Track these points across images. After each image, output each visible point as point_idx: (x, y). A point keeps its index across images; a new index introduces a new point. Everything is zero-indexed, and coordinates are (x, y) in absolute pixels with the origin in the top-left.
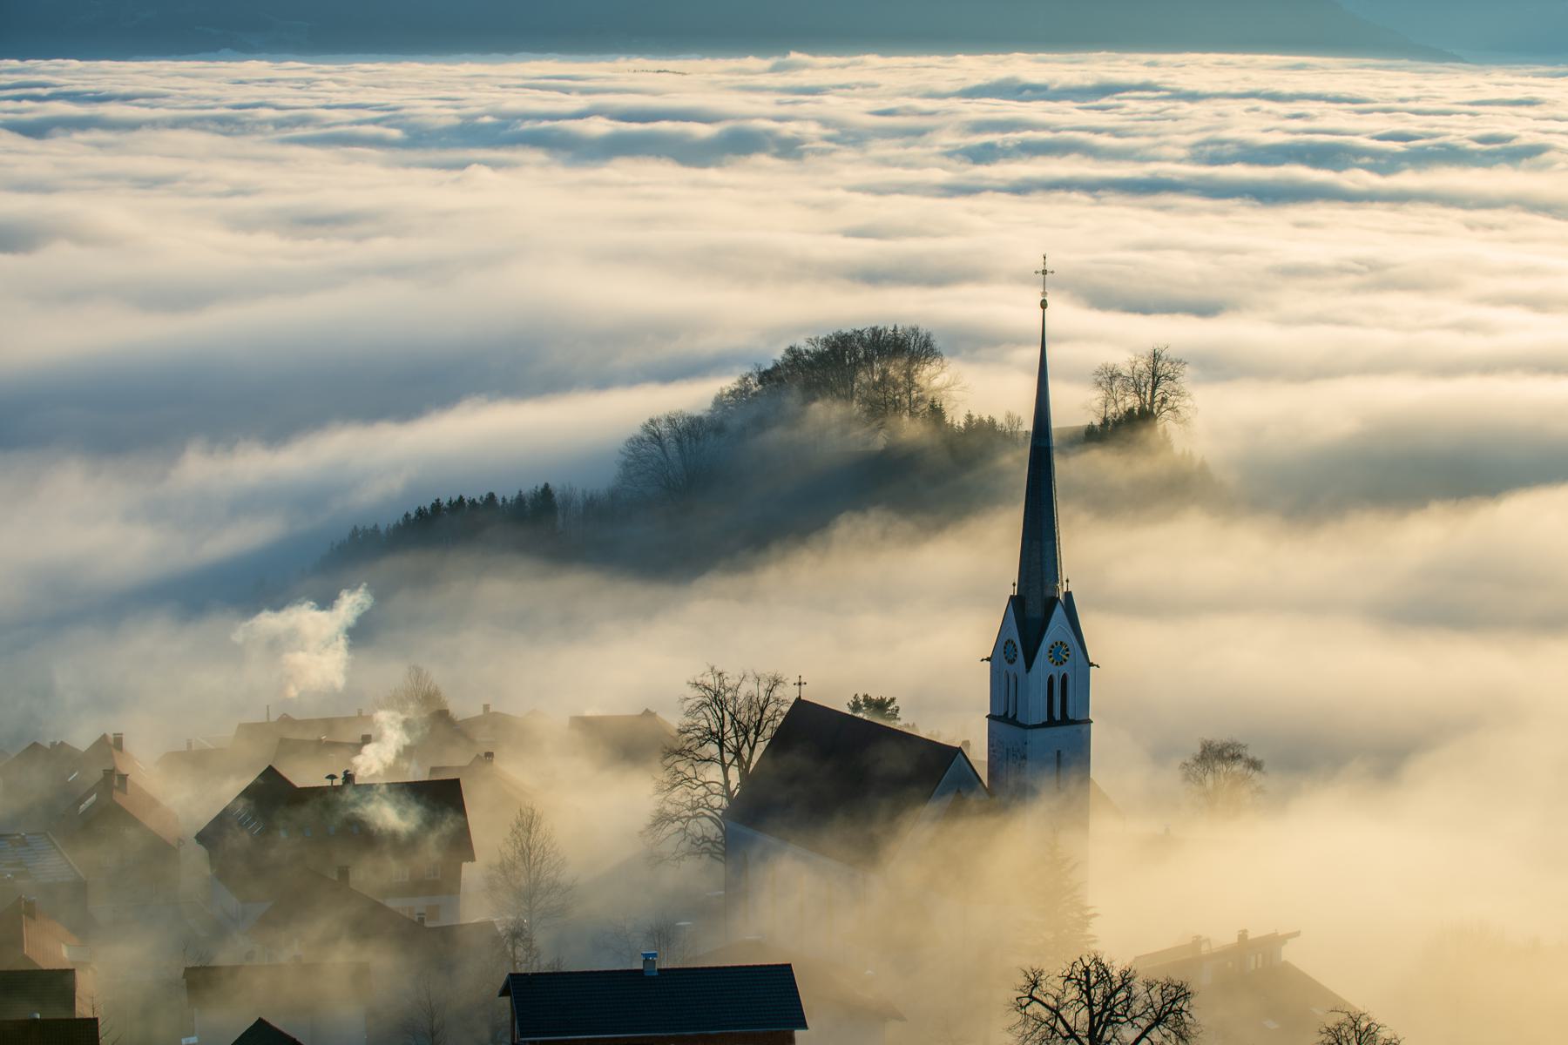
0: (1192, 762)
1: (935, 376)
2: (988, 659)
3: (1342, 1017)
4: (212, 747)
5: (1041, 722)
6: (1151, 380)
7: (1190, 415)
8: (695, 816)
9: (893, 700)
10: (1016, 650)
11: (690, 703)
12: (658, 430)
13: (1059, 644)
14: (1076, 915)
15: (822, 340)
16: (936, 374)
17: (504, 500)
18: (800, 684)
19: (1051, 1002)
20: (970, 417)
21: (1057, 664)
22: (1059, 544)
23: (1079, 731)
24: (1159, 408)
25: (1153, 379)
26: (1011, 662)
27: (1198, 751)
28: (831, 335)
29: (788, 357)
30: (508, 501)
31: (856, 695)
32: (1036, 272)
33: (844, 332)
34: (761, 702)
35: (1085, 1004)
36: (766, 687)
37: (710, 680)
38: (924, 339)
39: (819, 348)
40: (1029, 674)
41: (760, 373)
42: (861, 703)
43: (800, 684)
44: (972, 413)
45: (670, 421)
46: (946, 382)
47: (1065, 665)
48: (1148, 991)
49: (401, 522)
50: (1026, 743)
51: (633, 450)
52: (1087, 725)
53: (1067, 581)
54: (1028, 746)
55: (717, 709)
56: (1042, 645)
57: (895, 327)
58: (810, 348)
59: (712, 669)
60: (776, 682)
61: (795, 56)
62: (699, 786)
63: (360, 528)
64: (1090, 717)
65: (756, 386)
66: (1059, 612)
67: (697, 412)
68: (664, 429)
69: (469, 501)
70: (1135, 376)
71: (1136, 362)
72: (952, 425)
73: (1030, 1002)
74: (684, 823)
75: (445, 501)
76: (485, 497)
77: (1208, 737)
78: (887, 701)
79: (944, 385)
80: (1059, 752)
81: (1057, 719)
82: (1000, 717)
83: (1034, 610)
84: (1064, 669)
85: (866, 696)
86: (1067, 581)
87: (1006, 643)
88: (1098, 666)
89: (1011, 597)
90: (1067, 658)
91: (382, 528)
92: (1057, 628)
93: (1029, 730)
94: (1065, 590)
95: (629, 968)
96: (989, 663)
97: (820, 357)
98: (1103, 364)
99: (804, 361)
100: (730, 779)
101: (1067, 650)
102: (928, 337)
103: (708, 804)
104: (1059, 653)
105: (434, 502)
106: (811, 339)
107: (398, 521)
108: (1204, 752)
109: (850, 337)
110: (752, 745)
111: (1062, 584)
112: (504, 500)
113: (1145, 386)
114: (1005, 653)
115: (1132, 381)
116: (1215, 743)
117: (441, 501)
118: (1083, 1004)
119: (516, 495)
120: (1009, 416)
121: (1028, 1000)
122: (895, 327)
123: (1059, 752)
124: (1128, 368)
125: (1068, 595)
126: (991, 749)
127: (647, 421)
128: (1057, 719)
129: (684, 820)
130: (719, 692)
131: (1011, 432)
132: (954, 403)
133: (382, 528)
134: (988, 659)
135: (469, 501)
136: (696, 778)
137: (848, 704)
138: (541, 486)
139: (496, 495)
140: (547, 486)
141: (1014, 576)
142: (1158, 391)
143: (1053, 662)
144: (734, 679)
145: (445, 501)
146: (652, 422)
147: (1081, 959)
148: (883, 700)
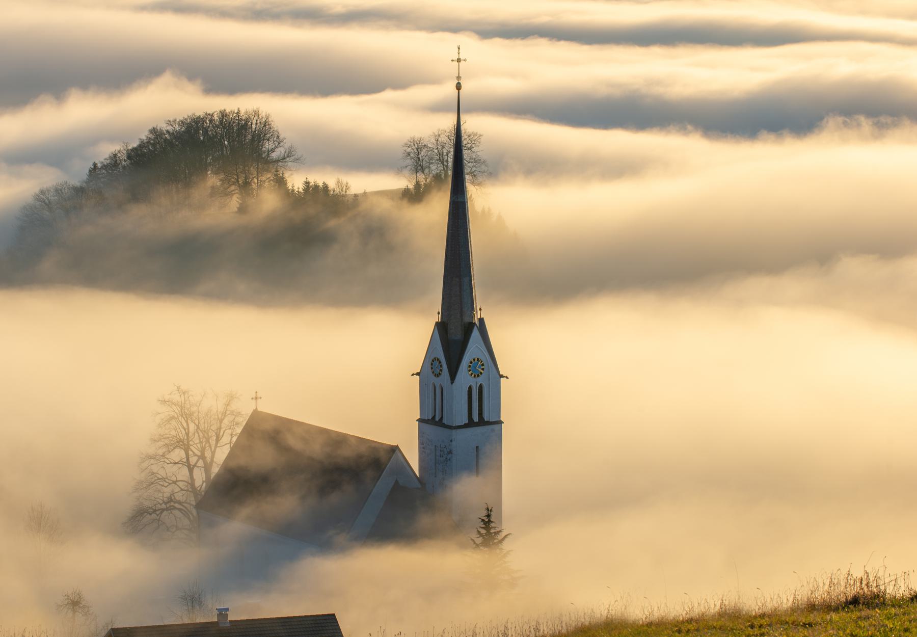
1: (273, 150)
5: (463, 424)
8: (167, 509)
10: (441, 366)
12: (48, 199)
13: (476, 361)
15: (179, 122)
16: (275, 148)
23: (493, 430)
28: (186, 117)
29: (152, 136)
32: (452, 61)
33: (198, 114)
34: (220, 416)
37: (177, 398)
38: (264, 120)
39: (177, 127)
40: (454, 384)
41: (127, 150)
47: (481, 377)
50: (451, 441)
52: (500, 425)
53: (480, 309)
54: (454, 443)
58: (170, 128)
59: (179, 389)
62: (171, 483)
65: (125, 161)
66: (476, 333)
70: (439, 148)
71: (439, 135)
72: (293, 190)
74: (157, 515)
81: (475, 421)
84: (480, 380)
86: (480, 309)
87: (433, 361)
88: (507, 378)
89: (437, 323)
90: (482, 371)
93: (454, 431)
94: (479, 317)
95: (210, 621)
96: (418, 377)
97: (176, 135)
99: (166, 139)
100: (195, 477)
101: (483, 365)
102: (267, 118)
104: (476, 368)
106: (169, 121)
111: (477, 313)
113: (447, 155)
114: (432, 368)
123: (477, 447)
124: (433, 140)
125: (481, 320)
126: (422, 446)
128: (475, 421)
129: (158, 512)
134: (418, 374)
143: (471, 375)
146: (42, 192)
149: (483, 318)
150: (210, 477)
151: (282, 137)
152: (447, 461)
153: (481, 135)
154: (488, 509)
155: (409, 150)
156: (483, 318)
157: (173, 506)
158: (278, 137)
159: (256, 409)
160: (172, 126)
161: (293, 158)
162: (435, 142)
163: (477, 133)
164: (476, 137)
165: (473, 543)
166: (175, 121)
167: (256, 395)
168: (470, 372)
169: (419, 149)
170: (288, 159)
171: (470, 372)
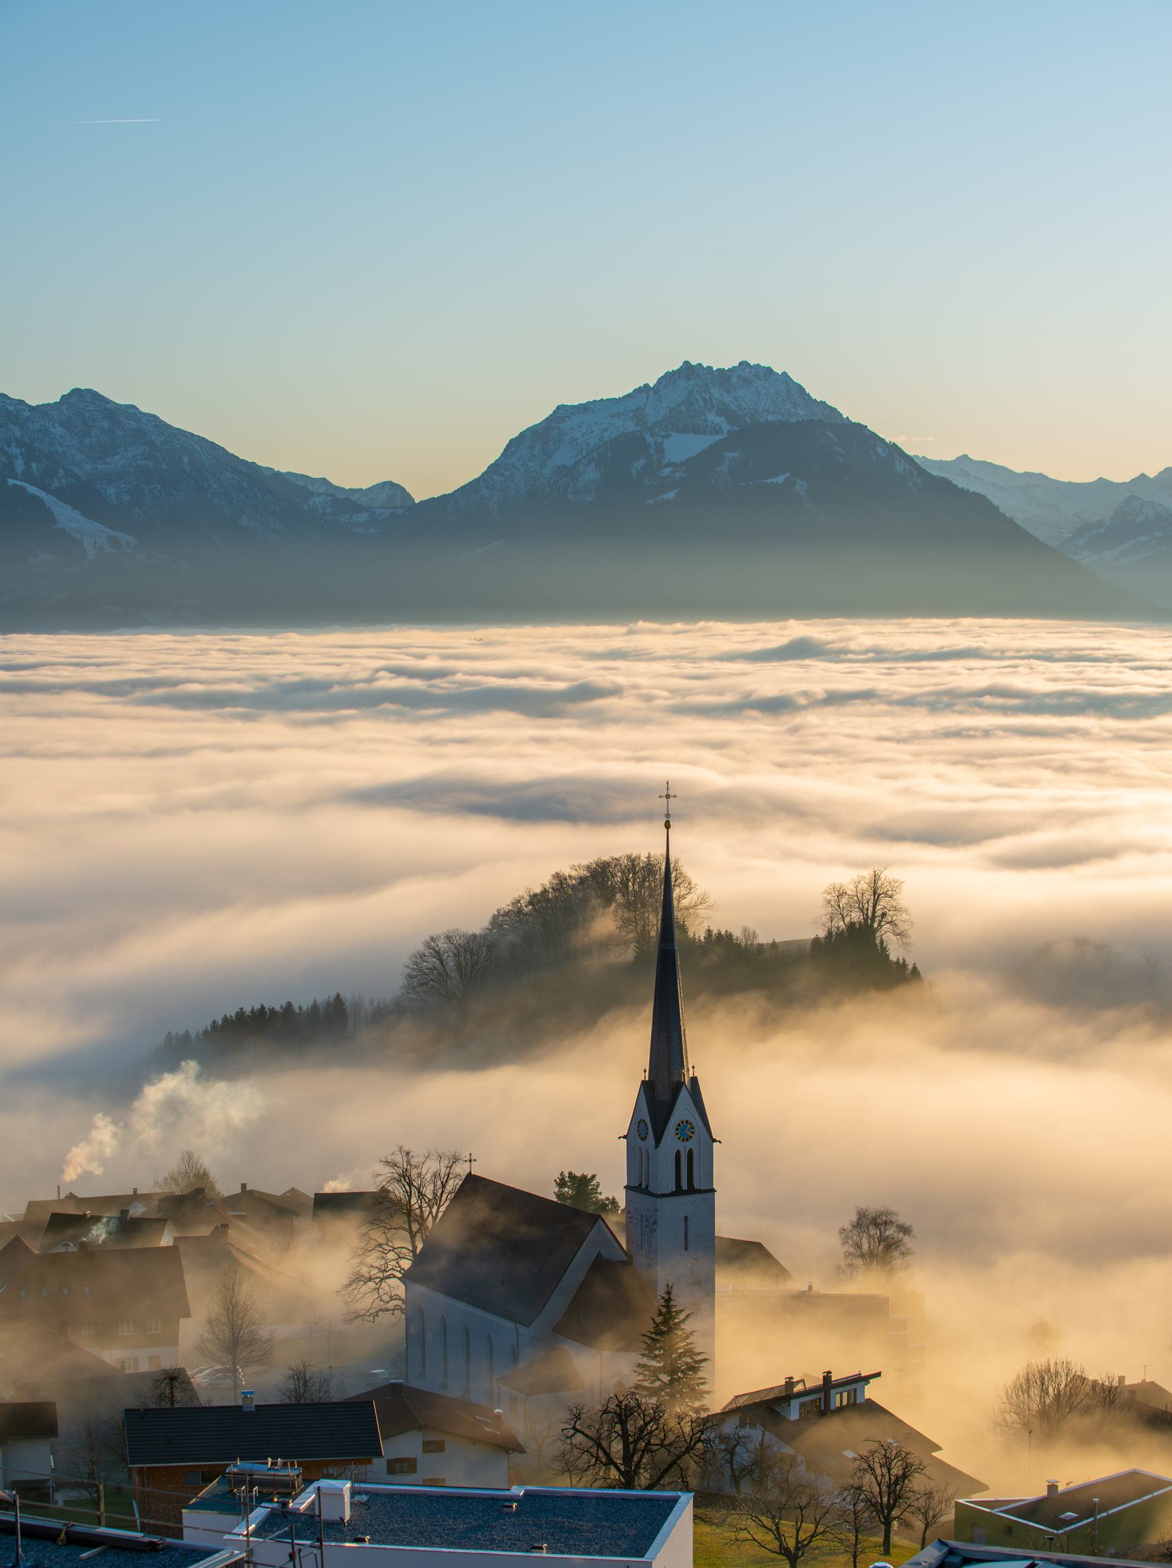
0: (850, 1227)
1: (684, 897)
2: (625, 1137)
3: (875, 1446)
4: (13, 1221)
5: (670, 1192)
6: (872, 897)
7: (906, 927)
9: (594, 1176)
10: (647, 1129)
11: (382, 1178)
13: (685, 1123)
14: (689, 1360)
17: (300, 1008)
18: (470, 1161)
19: (591, 1432)
20: (709, 931)
21: (683, 1140)
22: (685, 1035)
24: (881, 921)
25: (874, 896)
26: (644, 1139)
27: (854, 1218)
28: (592, 862)
29: (555, 881)
30: (305, 1009)
31: (562, 1172)
35: (619, 1435)
36: (446, 1164)
37: (398, 1159)
42: (567, 1179)
43: (470, 1161)
44: (711, 928)
45: (449, 938)
46: (694, 902)
48: (679, 1423)
49: (209, 1028)
50: (656, 1210)
51: (416, 964)
52: (712, 1193)
53: (693, 1067)
54: (659, 1213)
55: (405, 1183)
56: (669, 1123)
57: (649, 854)
58: (574, 873)
60: (456, 1159)
61: (641, 624)
62: (390, 1250)
63: (173, 1033)
64: (714, 1187)
65: (526, 906)
66: (684, 1095)
67: (478, 932)
68: (443, 945)
69: (269, 1009)
71: (859, 882)
73: (575, 1433)
74: (377, 1284)
75: (247, 1010)
76: (284, 1006)
77: (864, 1207)
78: (589, 1177)
79: (692, 904)
80: (686, 1218)
82: (635, 1187)
83: (663, 1094)
84: (690, 1145)
85: (570, 1174)
86: (693, 1067)
87: (639, 1123)
88: (720, 1142)
89: (643, 1082)
90: (692, 1135)
91: (193, 1034)
92: (683, 1110)
93: (659, 1199)
94: (691, 1075)
96: (625, 1140)
98: (831, 885)
101: (693, 1128)
103: (400, 1267)
104: (685, 1131)
105: (239, 1010)
106: (574, 866)
107: (207, 1027)
108: (859, 1219)
109: (608, 863)
110: (434, 1214)
111: (688, 1070)
112: (300, 1008)
114: (638, 1131)
115: (855, 898)
116: (869, 1211)
117: (244, 1010)
118: (616, 1435)
119: (311, 1003)
120: (745, 930)
121: (573, 1431)
122: (649, 854)
123: (686, 1218)
124: (852, 887)
125: (694, 1080)
127: (428, 938)
130: (406, 1169)
131: (746, 945)
132: (701, 920)
133: (193, 1034)
134: (625, 1137)
135: (269, 1009)
136: (387, 1244)
137: (555, 1181)
138: (333, 996)
139: (293, 1004)
140: (338, 995)
141: (646, 1065)
142: (878, 907)
143: (679, 1138)
144: (419, 1157)
145: (247, 1010)
146: (432, 939)
147: (616, 1396)
148: (584, 1177)
149: (696, 1077)
150: (39, 1254)
151: (693, 882)
152: (652, 1232)
153: (902, 882)
154: (668, 1285)
155: (829, 897)
156: (696, 1077)
157: (392, 1274)
158: (690, 883)
159: (470, 1172)
160: (576, 870)
161: (705, 905)
162: (854, 889)
163: (898, 880)
164: (897, 884)
165: (653, 1322)
166: (579, 866)
167: (470, 1157)
168: (678, 1136)
169: (841, 895)
170: (699, 907)
171: (678, 1136)
